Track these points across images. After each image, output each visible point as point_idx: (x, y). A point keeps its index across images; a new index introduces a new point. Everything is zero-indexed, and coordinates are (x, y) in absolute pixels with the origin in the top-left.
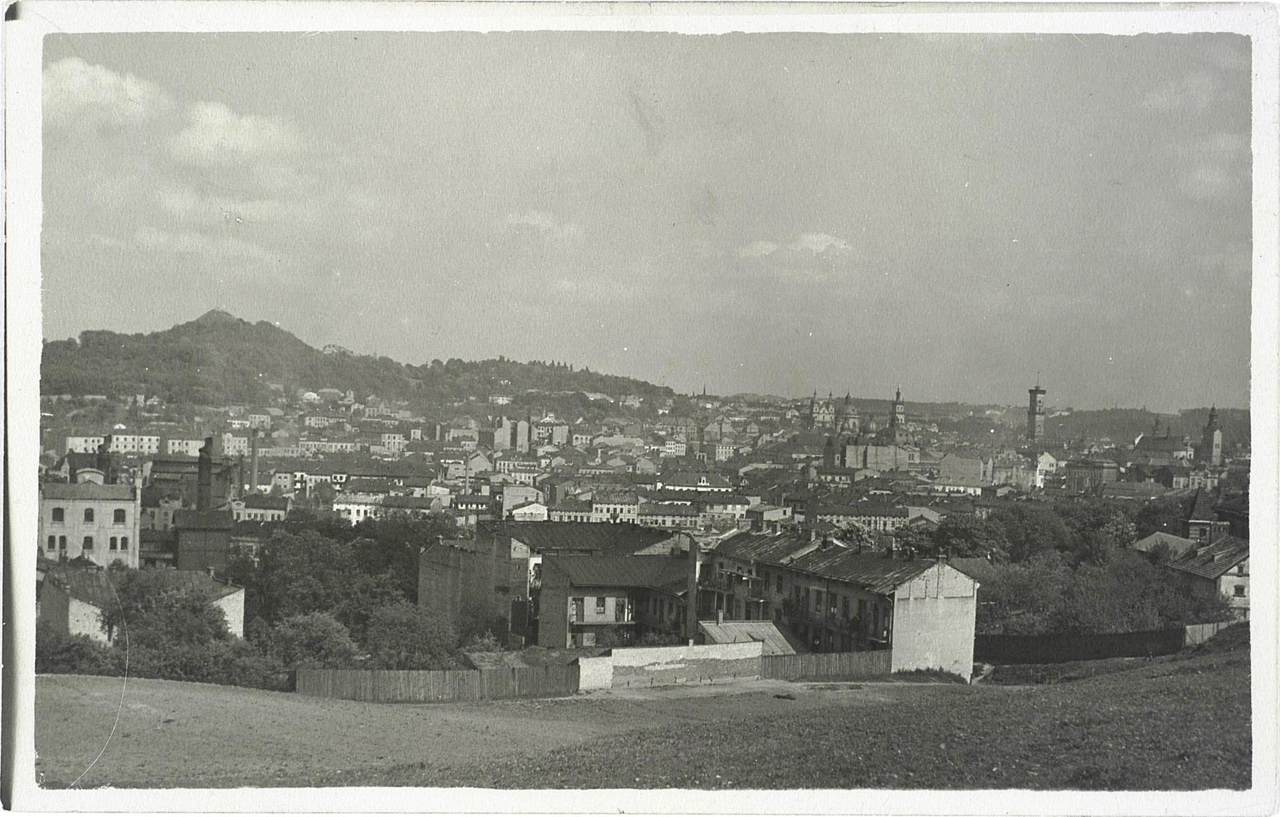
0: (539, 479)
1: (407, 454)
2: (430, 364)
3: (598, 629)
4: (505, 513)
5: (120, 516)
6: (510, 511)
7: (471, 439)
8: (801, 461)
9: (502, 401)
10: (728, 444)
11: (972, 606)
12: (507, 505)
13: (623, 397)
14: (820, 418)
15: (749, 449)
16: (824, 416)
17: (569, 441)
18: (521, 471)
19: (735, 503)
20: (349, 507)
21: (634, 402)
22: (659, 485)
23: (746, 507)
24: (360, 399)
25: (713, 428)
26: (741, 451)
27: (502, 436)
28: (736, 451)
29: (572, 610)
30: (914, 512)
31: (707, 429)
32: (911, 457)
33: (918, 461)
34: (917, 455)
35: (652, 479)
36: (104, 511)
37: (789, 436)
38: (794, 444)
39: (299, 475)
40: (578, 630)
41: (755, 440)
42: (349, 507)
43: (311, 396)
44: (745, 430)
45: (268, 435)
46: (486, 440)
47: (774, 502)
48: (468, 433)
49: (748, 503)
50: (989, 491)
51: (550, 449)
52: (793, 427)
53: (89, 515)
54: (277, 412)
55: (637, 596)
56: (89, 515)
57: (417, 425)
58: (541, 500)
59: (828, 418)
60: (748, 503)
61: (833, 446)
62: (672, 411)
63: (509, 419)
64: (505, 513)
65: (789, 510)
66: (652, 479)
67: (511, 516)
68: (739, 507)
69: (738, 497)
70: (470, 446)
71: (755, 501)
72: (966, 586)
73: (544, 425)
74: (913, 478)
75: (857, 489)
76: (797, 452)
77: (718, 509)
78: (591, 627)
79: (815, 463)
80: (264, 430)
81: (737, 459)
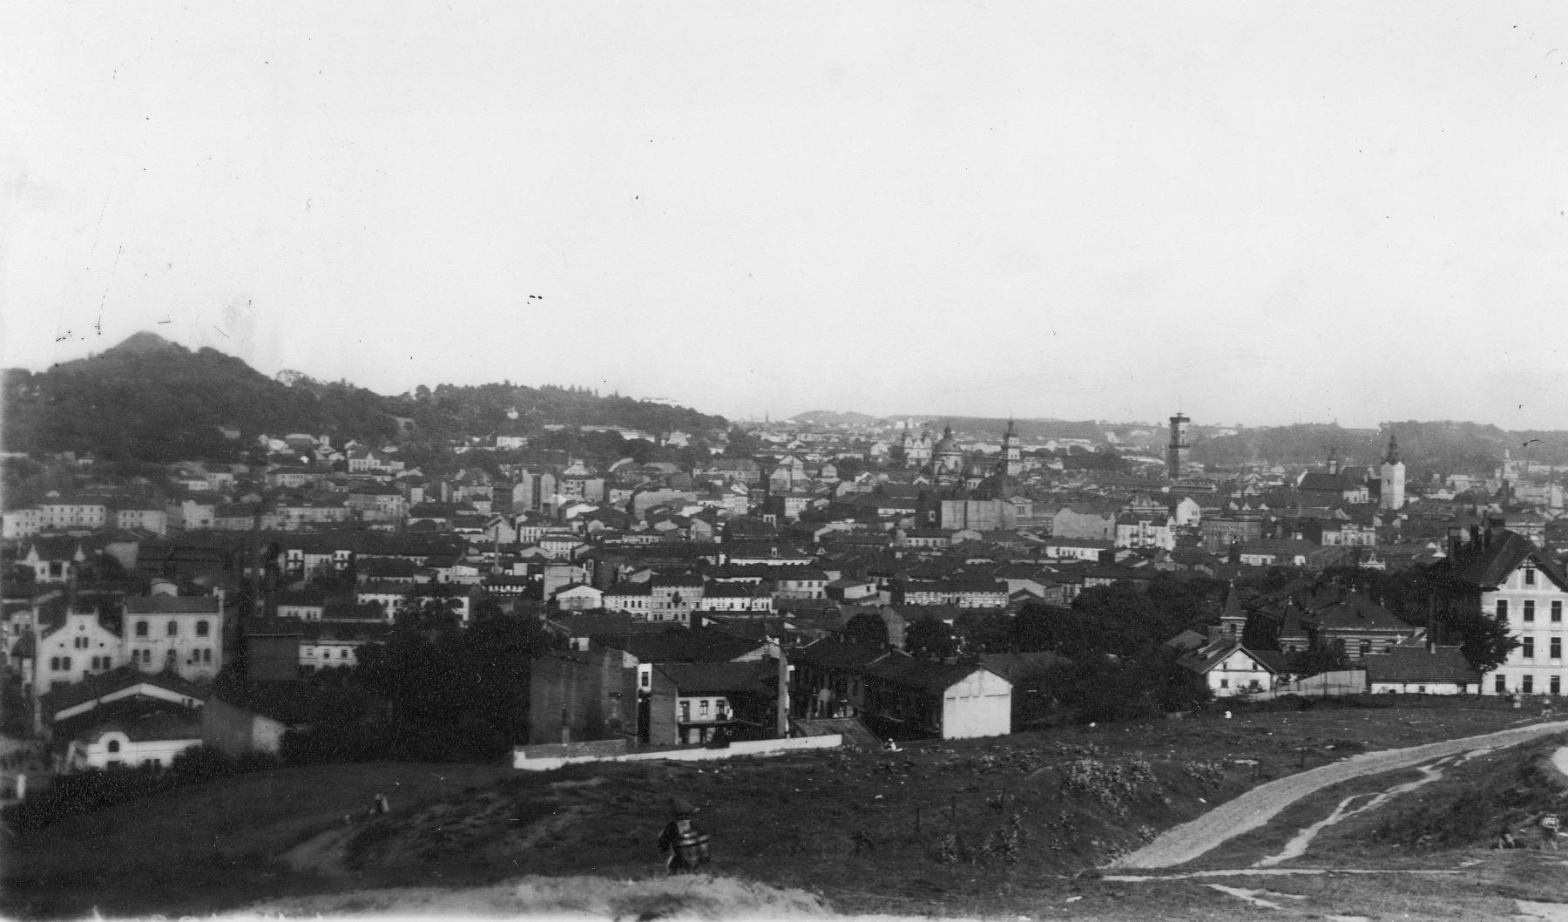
0: (578, 551)
1: (413, 521)
2: (413, 393)
3: (703, 727)
4: (547, 597)
5: (202, 629)
6: (553, 595)
7: (485, 498)
8: (888, 520)
9: (514, 443)
10: (801, 495)
11: (1007, 703)
12: (549, 588)
13: (665, 434)
14: (913, 454)
15: (824, 501)
16: (918, 451)
17: (606, 497)
18: (552, 540)
19: (811, 577)
20: (381, 598)
21: (679, 439)
22: (722, 558)
23: (825, 583)
24: (338, 446)
25: (779, 475)
26: (816, 504)
27: (521, 493)
28: (810, 503)
29: (679, 712)
30: (1015, 585)
31: (774, 476)
32: (1021, 510)
33: (1029, 515)
34: (1028, 508)
35: (714, 550)
36: (188, 622)
37: (873, 482)
38: (881, 494)
39: (292, 553)
40: (684, 729)
41: (833, 487)
42: (381, 598)
43: (277, 445)
44: (820, 475)
45: (236, 499)
46: (503, 501)
47: (853, 578)
48: (481, 491)
49: (826, 578)
50: (1107, 557)
51: (585, 509)
52: (882, 469)
53: (172, 629)
54: (242, 468)
55: (736, 698)
56: (172, 629)
57: (416, 482)
58: (588, 580)
59: (923, 454)
60: (826, 578)
61: (927, 502)
62: (728, 449)
63: (530, 471)
64: (547, 597)
65: (873, 587)
66: (714, 550)
67: (554, 601)
68: (815, 583)
69: (814, 572)
70: (483, 508)
71: (835, 576)
72: (1003, 686)
73: (573, 477)
74: (1021, 539)
75: (953, 556)
76: (885, 506)
77: (792, 584)
78: (696, 726)
79: (905, 522)
80: (230, 494)
81: (812, 517)
